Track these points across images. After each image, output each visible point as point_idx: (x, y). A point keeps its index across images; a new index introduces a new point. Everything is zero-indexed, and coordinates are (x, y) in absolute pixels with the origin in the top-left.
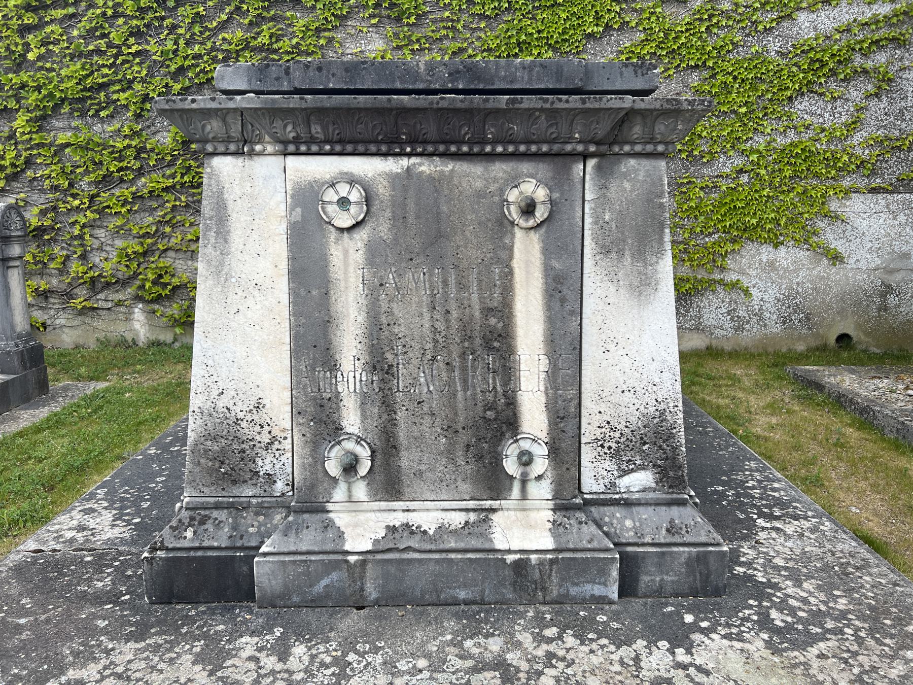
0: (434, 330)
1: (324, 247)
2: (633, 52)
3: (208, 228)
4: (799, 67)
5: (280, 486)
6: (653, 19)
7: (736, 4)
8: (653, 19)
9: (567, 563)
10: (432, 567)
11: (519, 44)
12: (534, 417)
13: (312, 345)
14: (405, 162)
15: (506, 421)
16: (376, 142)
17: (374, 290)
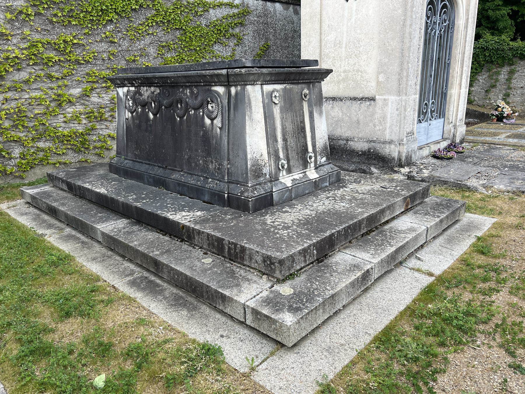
0: (293, 129)
1: (273, 108)
2: (153, 19)
3: (247, 106)
4: (213, 32)
5: (268, 176)
6: (159, 5)
7: (188, 2)
8: (159, 5)
9: (322, 179)
10: (303, 186)
11: (102, 10)
12: (310, 149)
13: (271, 137)
14: (284, 85)
15: (306, 150)
16: (282, 80)
17: (282, 119)
